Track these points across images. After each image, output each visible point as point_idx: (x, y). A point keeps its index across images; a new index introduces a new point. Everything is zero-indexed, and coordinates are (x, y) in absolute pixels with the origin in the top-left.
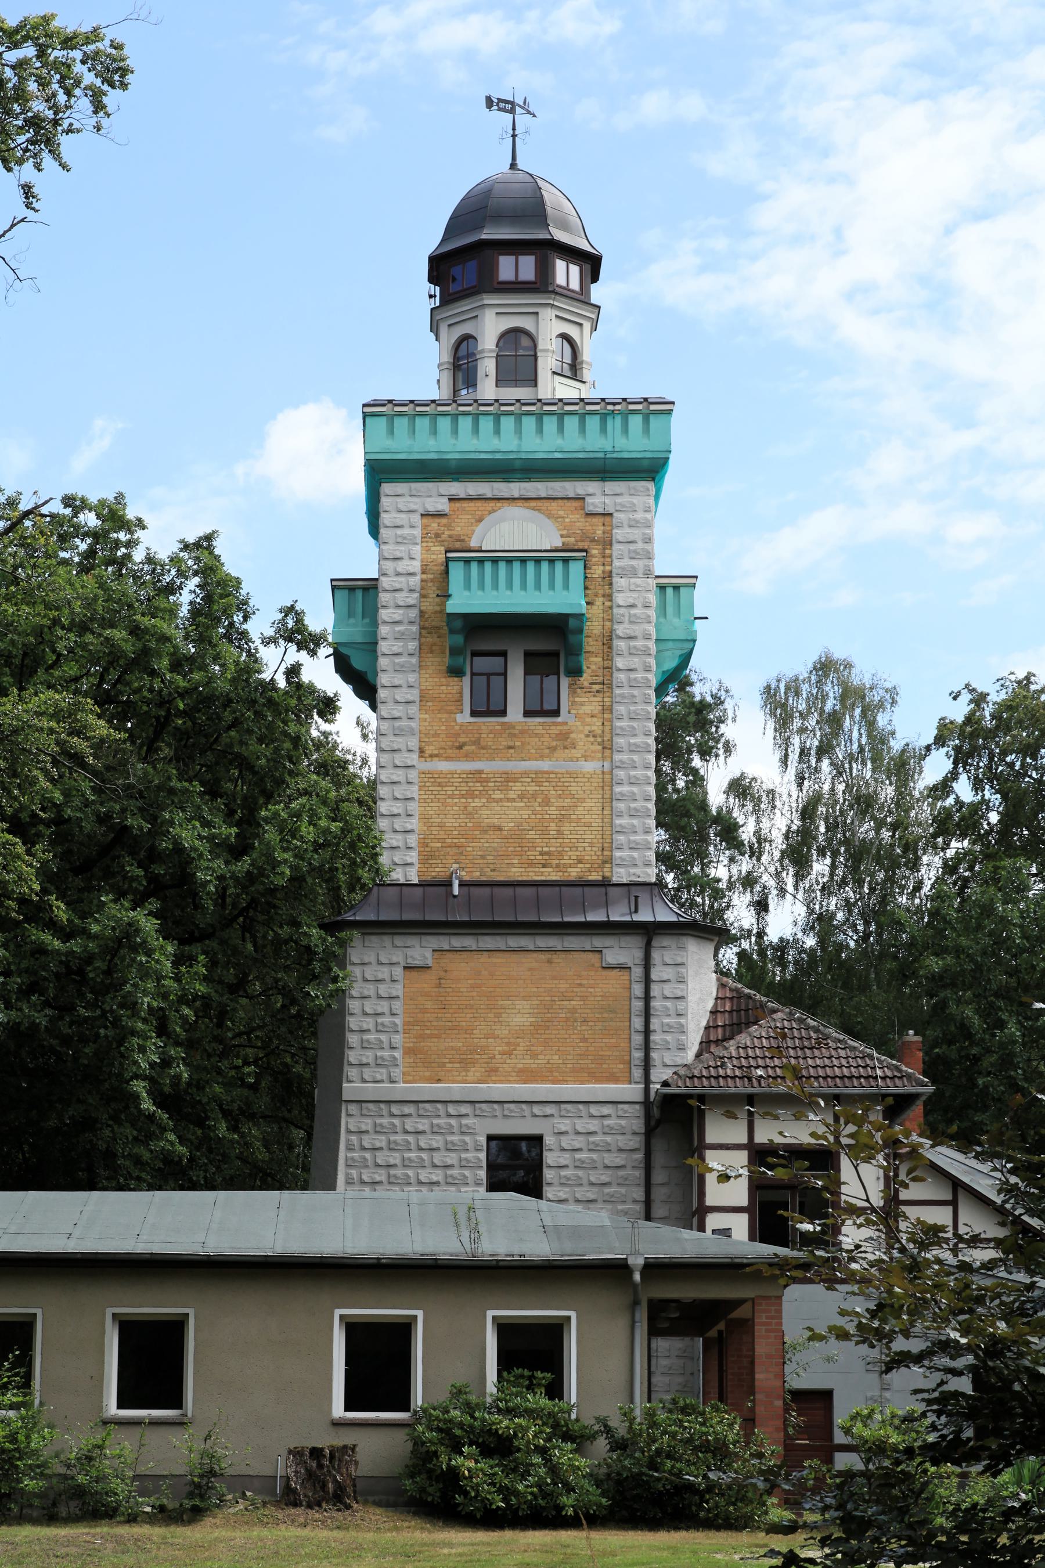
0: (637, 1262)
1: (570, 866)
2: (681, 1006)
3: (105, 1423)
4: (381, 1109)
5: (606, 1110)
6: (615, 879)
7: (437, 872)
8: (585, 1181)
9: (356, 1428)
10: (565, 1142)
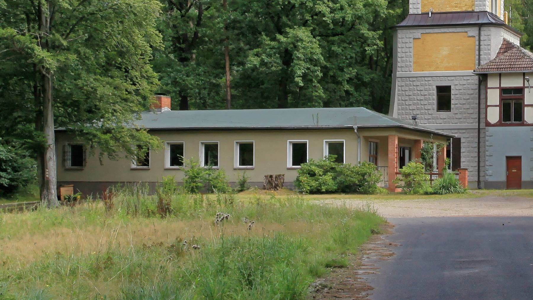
0: (355, 127)
1: (463, 7)
2: (489, 47)
3: (235, 169)
4: (407, 79)
5: (468, 78)
6: (475, 11)
7: (426, 11)
8: (462, 98)
9: (293, 170)
10: (457, 87)
